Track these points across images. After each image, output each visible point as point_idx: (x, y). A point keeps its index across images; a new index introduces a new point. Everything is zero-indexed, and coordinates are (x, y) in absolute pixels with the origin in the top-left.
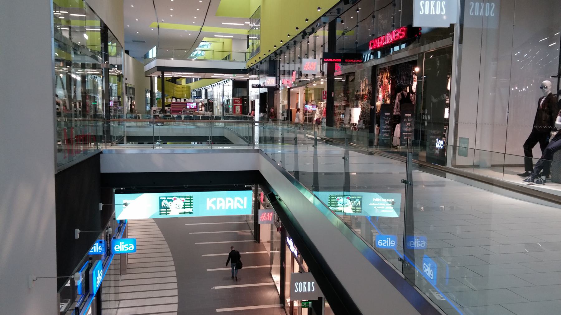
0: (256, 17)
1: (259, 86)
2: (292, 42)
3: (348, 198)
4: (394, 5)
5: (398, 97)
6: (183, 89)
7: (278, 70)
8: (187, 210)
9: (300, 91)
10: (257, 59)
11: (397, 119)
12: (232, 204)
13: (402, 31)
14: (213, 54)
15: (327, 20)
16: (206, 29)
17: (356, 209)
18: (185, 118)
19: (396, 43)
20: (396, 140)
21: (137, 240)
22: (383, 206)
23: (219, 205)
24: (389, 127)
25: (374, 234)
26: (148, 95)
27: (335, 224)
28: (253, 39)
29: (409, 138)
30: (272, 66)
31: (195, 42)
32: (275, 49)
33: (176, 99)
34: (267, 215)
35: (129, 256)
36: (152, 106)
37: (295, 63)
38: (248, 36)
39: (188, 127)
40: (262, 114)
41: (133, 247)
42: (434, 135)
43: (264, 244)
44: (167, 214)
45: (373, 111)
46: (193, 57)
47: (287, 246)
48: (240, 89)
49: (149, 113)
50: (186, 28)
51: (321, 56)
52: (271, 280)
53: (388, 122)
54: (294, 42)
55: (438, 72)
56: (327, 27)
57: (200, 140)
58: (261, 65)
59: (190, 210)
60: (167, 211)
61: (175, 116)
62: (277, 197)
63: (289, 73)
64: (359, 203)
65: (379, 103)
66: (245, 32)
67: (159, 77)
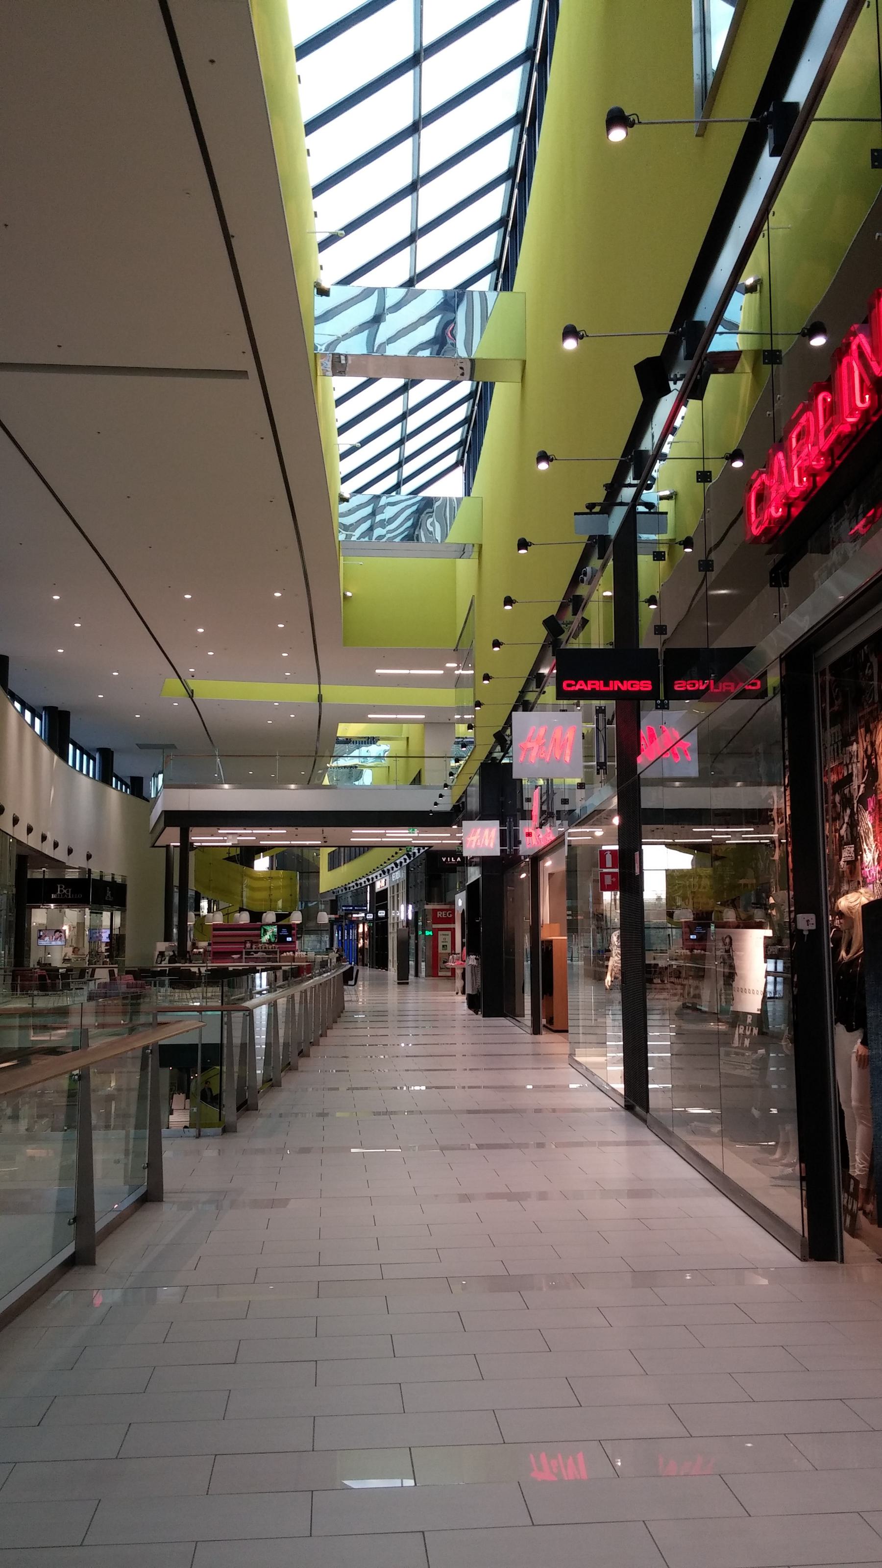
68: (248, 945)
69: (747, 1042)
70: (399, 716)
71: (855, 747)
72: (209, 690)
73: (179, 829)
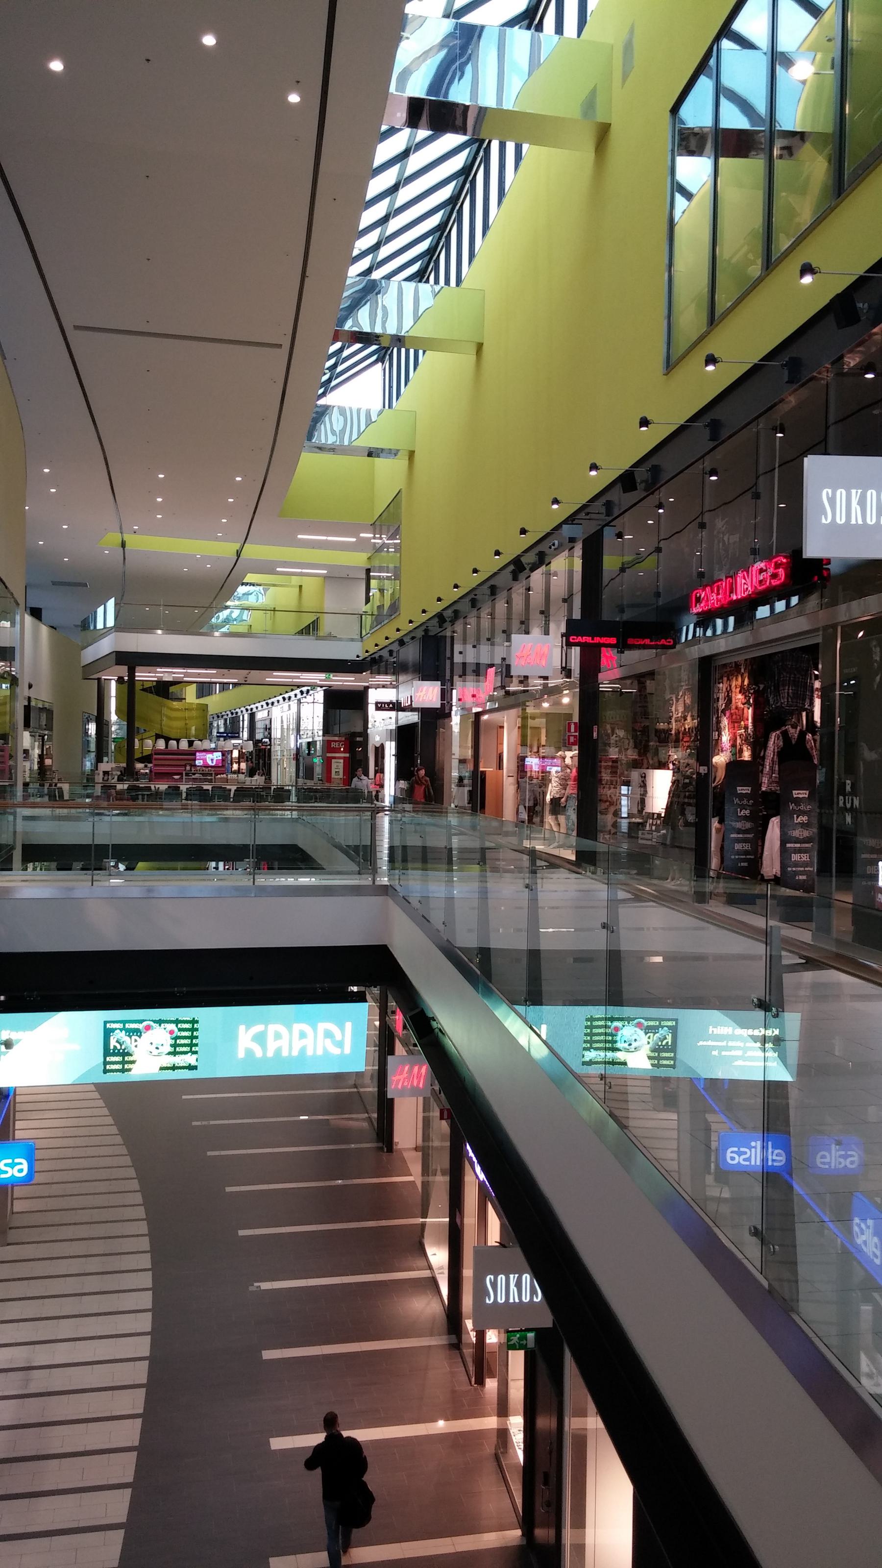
0: (389, 521)
1: (396, 706)
2: (486, 589)
3: (639, 1025)
4: (757, 496)
5: (774, 742)
6: (187, 714)
7: (448, 662)
8: (179, 1060)
9: (509, 720)
10: (390, 632)
11: (771, 805)
12: (309, 1042)
13: (777, 566)
14: (274, 619)
15: (578, 531)
16: (252, 551)
17: (659, 1058)
18: (190, 794)
19: (765, 597)
20: (771, 865)
21: (39, 1144)
22: (738, 1048)
23: (272, 1046)
24: (748, 825)
25: (714, 1127)
26: (92, 728)
27: (584, 1114)
28: (379, 578)
29: (805, 860)
30: (431, 653)
31: (223, 586)
32: (440, 606)
33: (167, 740)
34: (411, 1070)
35: (17, 1192)
36: (99, 759)
37: (493, 644)
38: (368, 571)
39: (196, 818)
40: (403, 784)
41: (25, 1166)
42: (873, 850)
43: (406, 1155)
44: (123, 1071)
45: (703, 781)
46: (218, 627)
47: (467, 1162)
48: (345, 713)
49: (90, 779)
50: (202, 549)
51: (563, 629)
52: (422, 1263)
53: (747, 812)
54: (492, 588)
55: (878, 678)
56: (578, 551)
57: (231, 854)
58: (403, 650)
59: (190, 1059)
60: (123, 1063)
61: (163, 787)
62: (434, 1024)
63: (478, 671)
64: (669, 1039)
65: (720, 759)
66: (360, 559)
67: (120, 680)
68: (188, 768)
69: (654, 828)
70: (304, 571)
71: (721, 685)
72: (138, 542)
73: (126, 667)
